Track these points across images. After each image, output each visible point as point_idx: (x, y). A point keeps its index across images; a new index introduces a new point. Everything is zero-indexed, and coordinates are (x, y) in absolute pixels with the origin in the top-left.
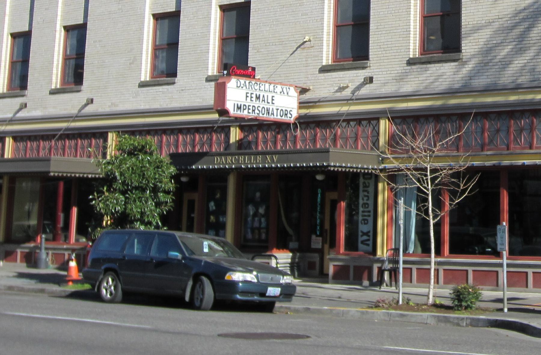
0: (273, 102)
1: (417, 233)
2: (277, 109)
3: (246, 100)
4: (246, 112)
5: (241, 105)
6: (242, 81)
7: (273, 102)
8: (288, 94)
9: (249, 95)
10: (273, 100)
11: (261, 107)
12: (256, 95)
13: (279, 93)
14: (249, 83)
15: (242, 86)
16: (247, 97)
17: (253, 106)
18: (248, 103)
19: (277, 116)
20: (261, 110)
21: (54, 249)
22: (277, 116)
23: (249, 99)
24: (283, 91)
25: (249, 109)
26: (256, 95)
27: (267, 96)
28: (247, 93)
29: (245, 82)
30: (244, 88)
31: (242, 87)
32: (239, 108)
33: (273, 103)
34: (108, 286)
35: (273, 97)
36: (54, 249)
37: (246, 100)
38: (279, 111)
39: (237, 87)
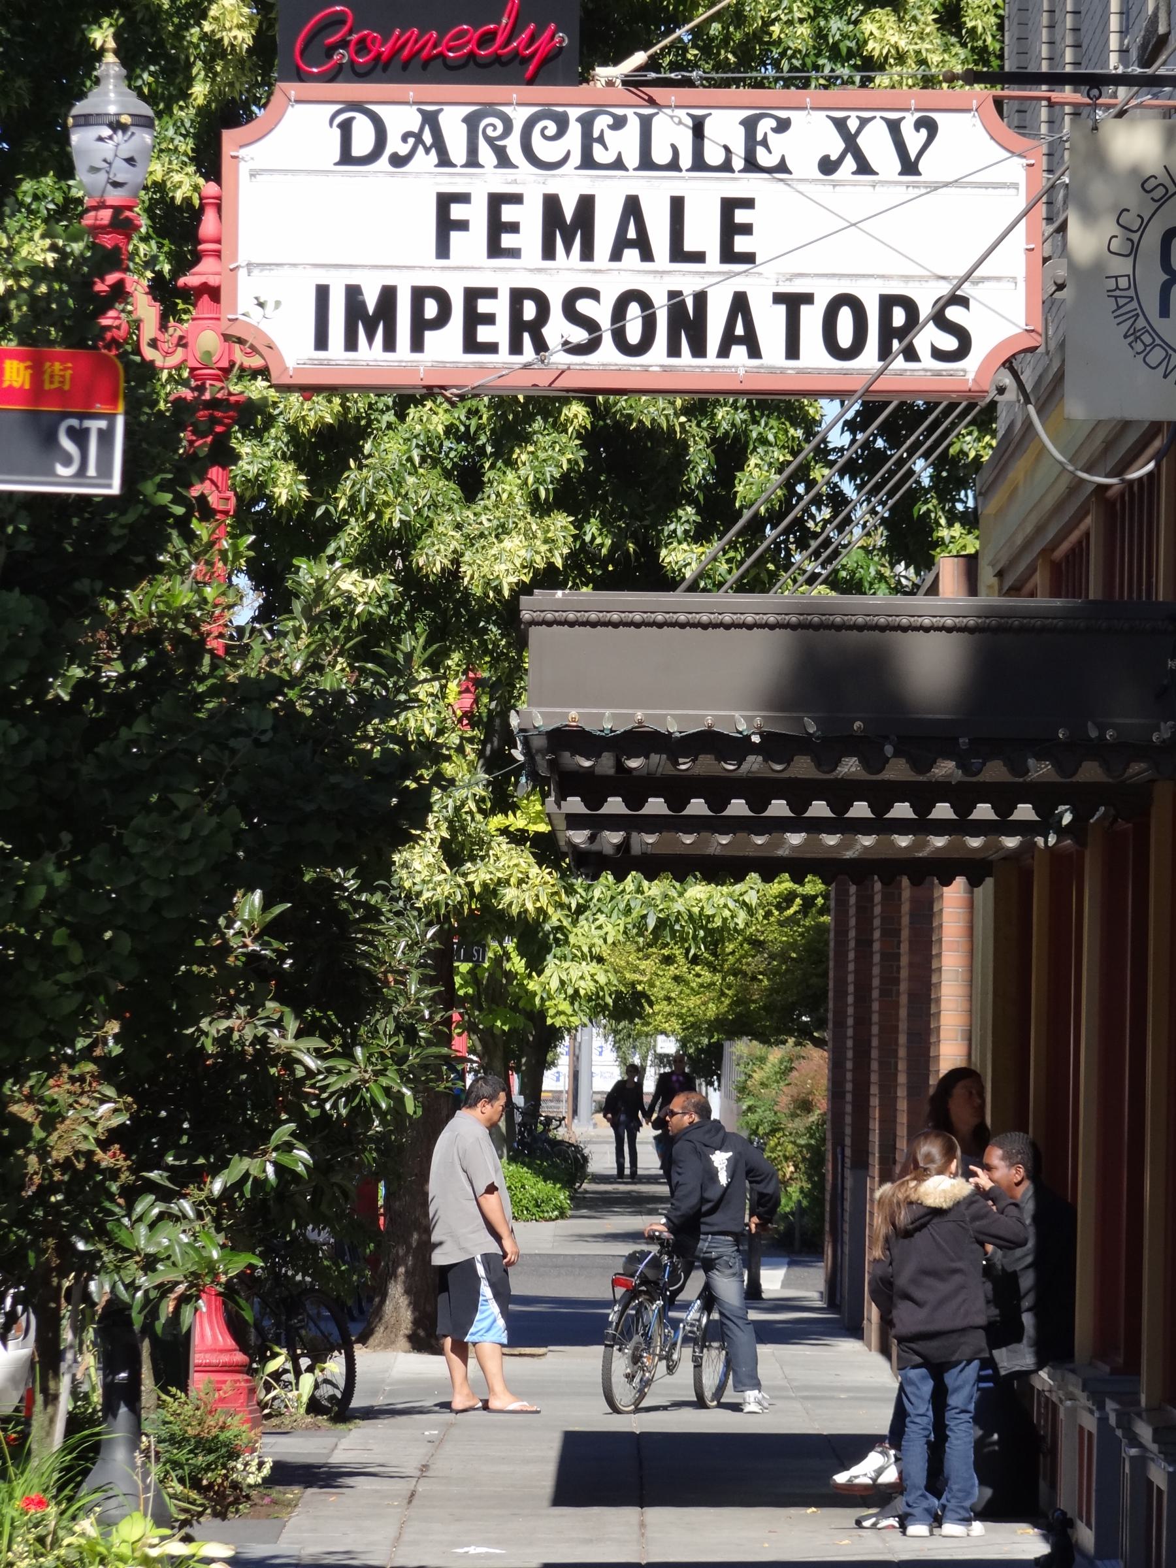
0: (741, 244)
1: (629, 1192)
2: (793, 303)
3: (443, 250)
4: (445, 344)
5: (388, 295)
6: (401, 119)
7: (741, 244)
8: (909, 167)
9: (476, 213)
10: (730, 229)
11: (609, 300)
12: (552, 204)
13: (804, 165)
14: (472, 122)
15: (395, 145)
16: (446, 226)
17: (518, 296)
18: (469, 264)
19: (793, 350)
20: (605, 322)
21: (841, 942)
22: (793, 350)
23: (470, 244)
24: (851, 145)
25: (473, 319)
26: (552, 204)
27: (677, 205)
28: (445, 201)
29: (431, 120)
30: (425, 161)
31: (398, 161)
32: (371, 317)
33: (729, 255)
34: (125, 603)
35: (729, 206)
36: (841, 942)
37: (443, 250)
38: (811, 319)
39: (346, 158)
